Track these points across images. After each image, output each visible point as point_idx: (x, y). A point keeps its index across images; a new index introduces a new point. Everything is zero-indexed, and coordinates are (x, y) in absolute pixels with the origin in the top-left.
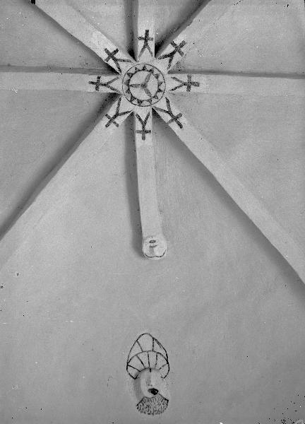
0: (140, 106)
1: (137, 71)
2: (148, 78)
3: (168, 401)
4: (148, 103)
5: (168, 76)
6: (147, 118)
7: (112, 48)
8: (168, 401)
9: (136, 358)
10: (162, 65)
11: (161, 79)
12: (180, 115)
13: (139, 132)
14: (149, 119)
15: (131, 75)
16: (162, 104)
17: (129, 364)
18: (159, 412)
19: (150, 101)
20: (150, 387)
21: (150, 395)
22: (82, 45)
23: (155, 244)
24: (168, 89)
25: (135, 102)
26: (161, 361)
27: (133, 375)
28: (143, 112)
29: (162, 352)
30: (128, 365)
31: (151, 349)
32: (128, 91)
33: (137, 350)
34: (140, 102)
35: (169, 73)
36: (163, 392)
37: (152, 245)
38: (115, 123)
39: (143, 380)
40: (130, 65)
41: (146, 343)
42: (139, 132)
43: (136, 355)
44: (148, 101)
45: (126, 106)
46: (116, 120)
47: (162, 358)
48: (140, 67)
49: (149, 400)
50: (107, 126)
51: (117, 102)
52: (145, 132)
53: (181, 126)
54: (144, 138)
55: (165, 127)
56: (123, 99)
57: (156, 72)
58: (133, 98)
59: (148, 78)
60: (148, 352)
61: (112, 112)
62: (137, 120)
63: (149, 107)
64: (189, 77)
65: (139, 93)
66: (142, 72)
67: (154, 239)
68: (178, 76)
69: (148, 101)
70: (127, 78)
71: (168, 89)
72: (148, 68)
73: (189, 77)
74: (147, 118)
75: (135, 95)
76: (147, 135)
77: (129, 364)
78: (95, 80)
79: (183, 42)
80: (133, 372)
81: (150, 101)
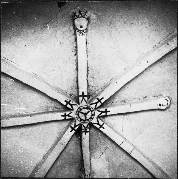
1: (79, 117)
2: (82, 113)
4: (93, 112)
5: (81, 105)
6: (82, 101)
7: (70, 129)
10: (76, 108)
11: (82, 108)
12: (98, 99)
13: (100, 102)
15: (81, 120)
16: (93, 106)
19: (92, 111)
22: (69, 141)
24: (86, 104)
25: (93, 117)
28: (97, 113)
32: (88, 120)
34: (93, 115)
35: (79, 104)
37: (161, 105)
38: (102, 125)
40: (77, 121)
42: (100, 102)
44: (92, 112)
45: (94, 121)
48: (77, 116)
50: (104, 128)
52: (99, 101)
54: (109, 111)
55: (106, 103)
56: (91, 122)
58: (91, 118)
59: (82, 113)
61: (98, 126)
63: (95, 111)
64: (80, 96)
65: (89, 116)
67: (159, 105)
68: (80, 101)
69: (92, 112)
71: (86, 104)
73: (80, 96)
74: (82, 101)
78: (84, 133)
79: (65, 101)
81: (92, 111)
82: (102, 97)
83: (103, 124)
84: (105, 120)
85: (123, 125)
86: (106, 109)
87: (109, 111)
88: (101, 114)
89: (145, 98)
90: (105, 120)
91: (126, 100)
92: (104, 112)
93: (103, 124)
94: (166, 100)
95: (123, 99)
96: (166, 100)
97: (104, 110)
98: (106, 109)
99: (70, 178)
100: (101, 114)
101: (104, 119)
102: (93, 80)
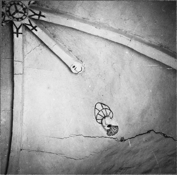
0: (23, 20)
1: (9, 7)
3: (118, 126)
8: (118, 126)
9: (98, 115)
13: (39, 17)
14: (31, 22)
15: (8, 11)
16: (31, 13)
17: (97, 119)
18: (116, 133)
19: (24, 15)
20: (107, 125)
21: (109, 128)
23: (75, 67)
25: (20, 20)
26: (108, 111)
27: (100, 122)
29: (107, 107)
30: (97, 120)
31: (102, 108)
32: (14, 18)
33: (97, 111)
34: (22, 19)
36: (113, 124)
38: (20, 33)
39: (104, 124)
41: (99, 107)
42: (39, 17)
43: (98, 114)
44: (24, 16)
46: (19, 32)
47: (108, 110)
48: (9, 5)
49: (109, 130)
51: (14, 25)
53: (44, 16)
54: (36, 30)
57: (16, 2)
60: (101, 110)
61: (15, 30)
62: (27, 26)
63: (27, 18)
66: (11, 7)
69: (24, 16)
70: (8, 13)
72: (12, 3)
75: (18, 17)
76: (36, 28)
77: (97, 119)
80: (100, 121)
82: (45, 15)
83: (21, 33)
84: (25, 32)
86: (36, 27)
87: (36, 30)
90: (25, 32)
92: (32, 26)
93: (21, 33)
101: (26, 30)
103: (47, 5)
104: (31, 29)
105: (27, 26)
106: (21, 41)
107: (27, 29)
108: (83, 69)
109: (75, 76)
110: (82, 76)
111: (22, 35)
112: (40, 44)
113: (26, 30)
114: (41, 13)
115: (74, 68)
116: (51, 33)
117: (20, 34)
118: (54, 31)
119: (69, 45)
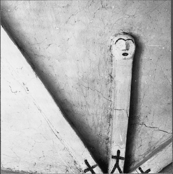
13: (94, 167)
14: (112, 169)
23: (124, 52)
42: (94, 167)
54: (119, 152)
67: (124, 57)
82: (84, 163)
83: (140, 169)
84: (138, 161)
85: (156, 129)
86: (113, 157)
87: (119, 152)
88: (119, 170)
89: (111, 77)
90: (138, 161)
91: (109, 113)
92: (117, 162)
93: (140, 169)
94: (117, 41)
95: (104, 120)
96: (117, 41)
97: (112, 163)
98: (113, 157)
99: (172, 16)
100: (119, 170)
101: (135, 162)
102: (55, 168)
103: (73, 165)
104: (124, 161)
105: (122, 169)
106: (151, 161)
107: (133, 160)
108: (117, 39)
109: (142, 35)
110: (132, 28)
111: (142, 167)
112: (140, 126)
113: (135, 162)
114: (85, 170)
115: (127, 52)
116: (110, 125)
117: (142, 169)
118: (101, 125)
119: (104, 85)
